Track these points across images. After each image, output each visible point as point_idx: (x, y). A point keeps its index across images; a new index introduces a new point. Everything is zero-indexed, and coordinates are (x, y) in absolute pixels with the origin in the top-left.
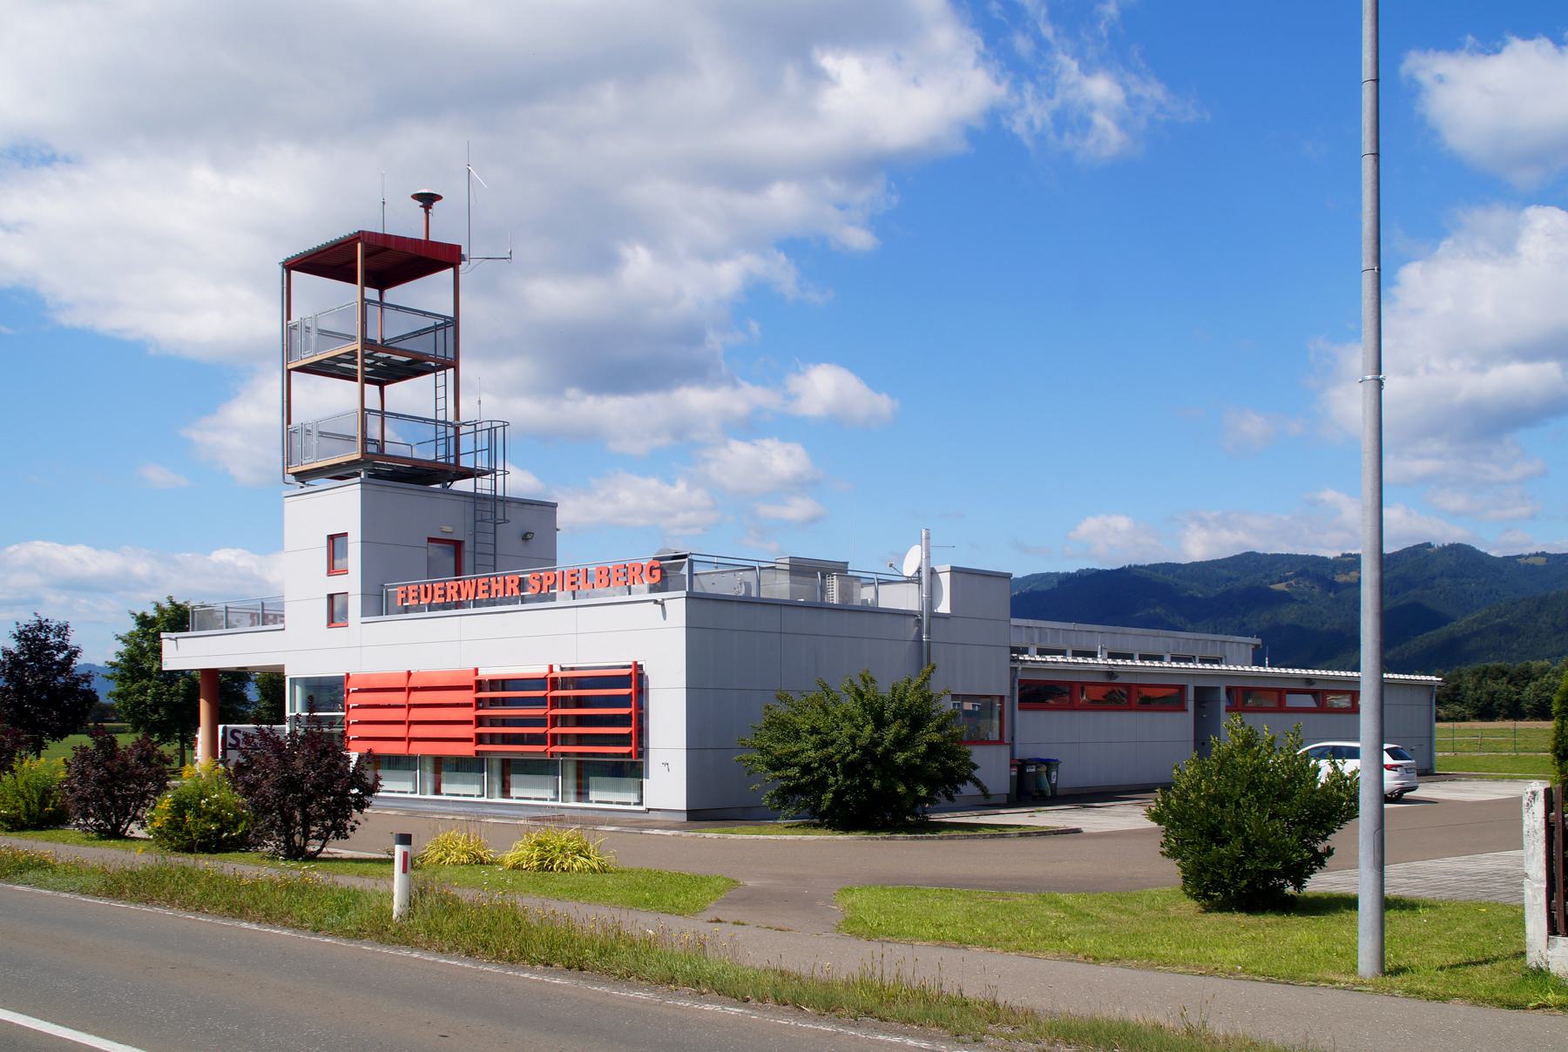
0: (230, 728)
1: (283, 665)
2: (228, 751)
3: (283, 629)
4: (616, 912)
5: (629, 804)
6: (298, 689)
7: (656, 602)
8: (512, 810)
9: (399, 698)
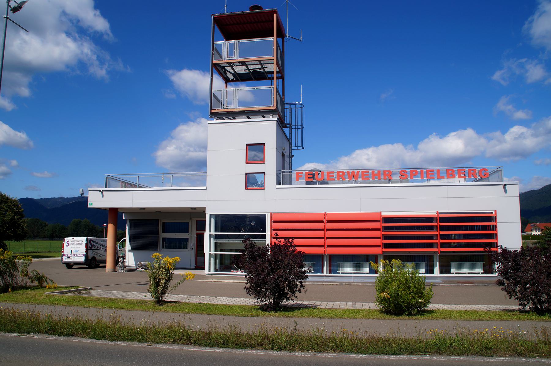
0: (89, 239)
1: (205, 208)
2: (89, 251)
3: (206, 189)
4: (31, 306)
5: (479, 273)
6: (213, 220)
7: (100, 191)
8: (369, 279)
9: (321, 226)
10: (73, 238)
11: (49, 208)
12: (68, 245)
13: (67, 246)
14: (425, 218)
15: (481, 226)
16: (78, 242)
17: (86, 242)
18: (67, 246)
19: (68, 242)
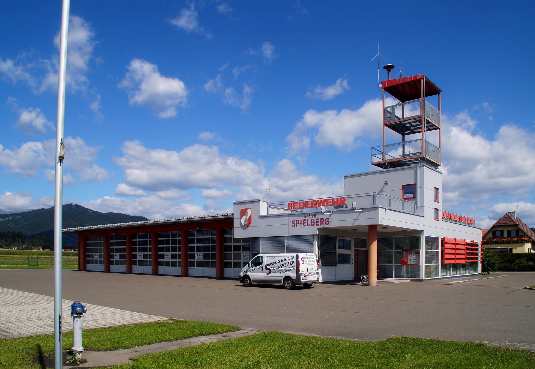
10: (307, 255)
11: (194, 205)
12: (303, 262)
13: (302, 264)
14: (380, 278)
15: (242, 239)
16: (312, 259)
17: (299, 259)
18: (302, 264)
19: (303, 259)
